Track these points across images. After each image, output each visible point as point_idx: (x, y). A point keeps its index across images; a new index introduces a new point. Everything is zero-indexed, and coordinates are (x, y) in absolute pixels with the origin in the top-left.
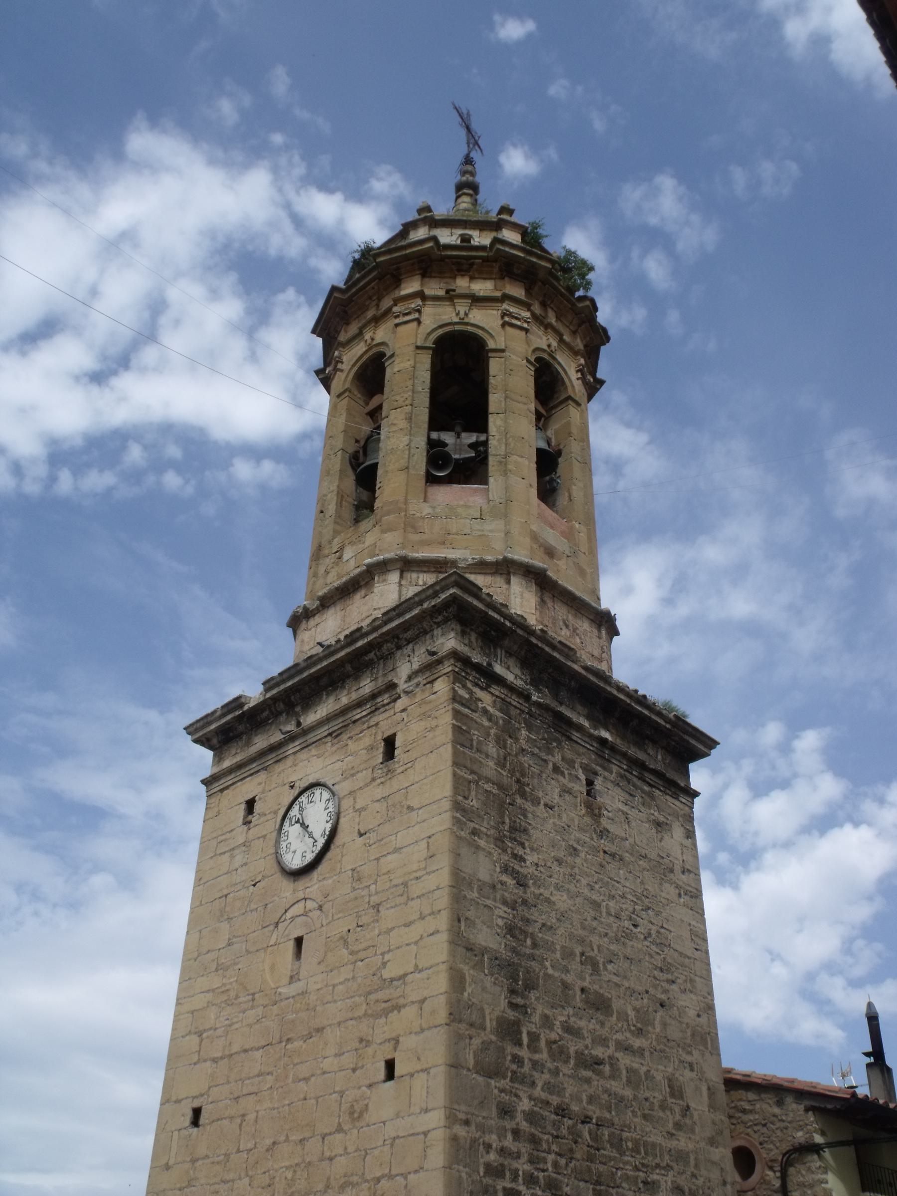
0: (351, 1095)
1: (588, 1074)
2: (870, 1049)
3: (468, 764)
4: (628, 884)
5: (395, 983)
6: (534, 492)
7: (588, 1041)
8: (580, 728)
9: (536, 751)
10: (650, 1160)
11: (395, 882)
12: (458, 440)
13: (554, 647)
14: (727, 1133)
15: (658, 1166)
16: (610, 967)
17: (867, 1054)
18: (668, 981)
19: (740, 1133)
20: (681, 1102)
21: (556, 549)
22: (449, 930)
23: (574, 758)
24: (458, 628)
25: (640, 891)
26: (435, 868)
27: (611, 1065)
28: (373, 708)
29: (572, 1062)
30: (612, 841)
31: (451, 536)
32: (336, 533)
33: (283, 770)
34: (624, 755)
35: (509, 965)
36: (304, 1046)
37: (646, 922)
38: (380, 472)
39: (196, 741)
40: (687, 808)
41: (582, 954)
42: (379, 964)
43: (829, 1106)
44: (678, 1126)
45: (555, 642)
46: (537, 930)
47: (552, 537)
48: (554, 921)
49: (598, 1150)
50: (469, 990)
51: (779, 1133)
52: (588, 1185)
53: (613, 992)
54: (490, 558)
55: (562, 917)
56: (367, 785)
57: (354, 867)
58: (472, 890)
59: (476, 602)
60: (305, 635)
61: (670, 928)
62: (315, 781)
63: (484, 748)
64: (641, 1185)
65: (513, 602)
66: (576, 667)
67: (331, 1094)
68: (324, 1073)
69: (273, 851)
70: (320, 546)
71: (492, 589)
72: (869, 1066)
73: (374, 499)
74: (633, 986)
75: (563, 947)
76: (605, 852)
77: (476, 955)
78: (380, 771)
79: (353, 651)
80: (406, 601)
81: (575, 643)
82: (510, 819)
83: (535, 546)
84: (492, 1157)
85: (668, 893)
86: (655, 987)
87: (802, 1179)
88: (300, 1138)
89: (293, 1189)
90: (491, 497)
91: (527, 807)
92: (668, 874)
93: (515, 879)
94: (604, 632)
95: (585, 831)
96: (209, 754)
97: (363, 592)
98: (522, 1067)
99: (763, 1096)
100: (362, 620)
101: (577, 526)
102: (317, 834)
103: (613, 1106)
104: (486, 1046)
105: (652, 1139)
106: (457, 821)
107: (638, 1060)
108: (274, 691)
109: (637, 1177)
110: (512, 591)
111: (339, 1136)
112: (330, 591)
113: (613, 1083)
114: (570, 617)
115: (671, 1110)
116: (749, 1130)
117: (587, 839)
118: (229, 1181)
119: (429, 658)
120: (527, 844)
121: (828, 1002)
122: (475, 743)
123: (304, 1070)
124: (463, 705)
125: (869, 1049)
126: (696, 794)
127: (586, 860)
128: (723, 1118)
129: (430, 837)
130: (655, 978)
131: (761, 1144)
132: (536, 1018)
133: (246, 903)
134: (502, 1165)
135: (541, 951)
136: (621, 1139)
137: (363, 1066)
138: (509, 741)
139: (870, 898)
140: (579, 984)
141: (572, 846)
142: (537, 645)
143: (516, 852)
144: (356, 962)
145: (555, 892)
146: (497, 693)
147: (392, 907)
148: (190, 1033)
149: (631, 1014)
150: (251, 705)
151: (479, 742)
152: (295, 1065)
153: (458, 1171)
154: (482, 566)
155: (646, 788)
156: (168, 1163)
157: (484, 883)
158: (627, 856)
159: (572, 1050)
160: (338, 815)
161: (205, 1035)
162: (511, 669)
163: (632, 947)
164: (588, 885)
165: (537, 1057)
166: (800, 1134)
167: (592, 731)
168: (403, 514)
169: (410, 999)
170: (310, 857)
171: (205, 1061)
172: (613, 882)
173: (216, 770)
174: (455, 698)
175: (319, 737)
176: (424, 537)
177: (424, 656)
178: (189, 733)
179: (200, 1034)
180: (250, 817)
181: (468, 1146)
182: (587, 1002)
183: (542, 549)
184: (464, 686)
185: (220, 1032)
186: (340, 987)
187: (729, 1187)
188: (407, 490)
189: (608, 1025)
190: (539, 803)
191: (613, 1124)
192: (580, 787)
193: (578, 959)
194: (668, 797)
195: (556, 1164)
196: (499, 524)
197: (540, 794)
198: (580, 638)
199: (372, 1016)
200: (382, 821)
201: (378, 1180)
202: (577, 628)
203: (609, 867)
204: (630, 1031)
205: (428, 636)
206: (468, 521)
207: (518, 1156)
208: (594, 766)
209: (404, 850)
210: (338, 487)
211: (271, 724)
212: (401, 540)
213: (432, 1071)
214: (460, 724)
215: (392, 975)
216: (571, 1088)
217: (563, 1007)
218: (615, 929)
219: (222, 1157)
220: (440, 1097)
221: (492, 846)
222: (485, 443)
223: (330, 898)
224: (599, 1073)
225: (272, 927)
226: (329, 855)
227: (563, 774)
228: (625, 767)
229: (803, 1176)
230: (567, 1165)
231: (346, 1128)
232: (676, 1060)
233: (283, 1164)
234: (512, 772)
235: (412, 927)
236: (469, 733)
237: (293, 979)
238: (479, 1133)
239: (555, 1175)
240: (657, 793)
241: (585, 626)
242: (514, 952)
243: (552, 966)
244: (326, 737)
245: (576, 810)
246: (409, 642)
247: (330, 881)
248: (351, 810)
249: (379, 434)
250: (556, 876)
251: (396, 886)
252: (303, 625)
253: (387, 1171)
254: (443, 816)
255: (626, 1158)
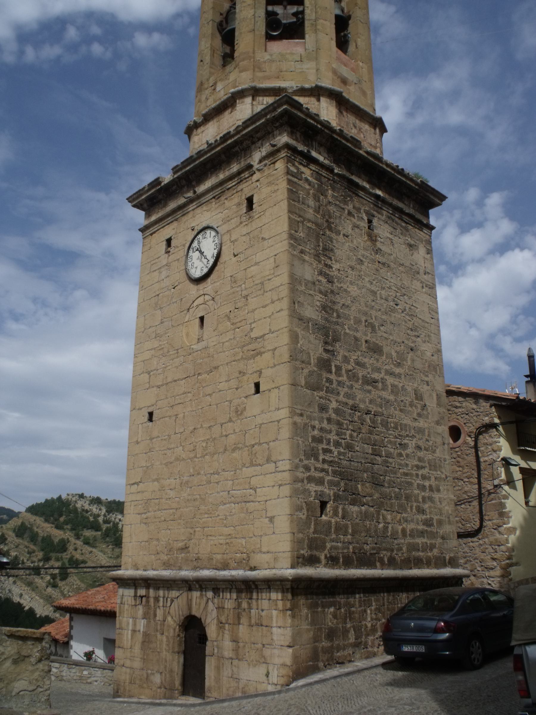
0: (236, 402)
1: (370, 388)
2: (528, 373)
3: (297, 211)
4: (392, 281)
5: (258, 340)
6: (334, 43)
7: (370, 370)
8: (363, 189)
9: (338, 203)
10: (403, 433)
11: (256, 282)
12: (285, 11)
13: (347, 140)
14: (446, 418)
15: (407, 436)
16: (382, 328)
17: (527, 376)
18: (415, 336)
19: (454, 419)
20: (421, 402)
21: (348, 79)
22: (289, 309)
23: (361, 207)
24: (289, 129)
25: (400, 285)
26: (279, 274)
27: (383, 383)
28: (239, 180)
29: (360, 381)
30: (383, 256)
31: (283, 73)
32: (211, 74)
33: (187, 220)
34: (391, 205)
35: (324, 328)
36: (208, 377)
37: (403, 303)
38: (237, 34)
39: (134, 206)
40: (427, 236)
41: (366, 321)
42: (249, 329)
43: (504, 404)
44: (419, 415)
45: (348, 137)
46: (339, 308)
47: (345, 72)
48: (349, 302)
49: (375, 428)
50: (301, 342)
51: (475, 418)
52: (369, 446)
53: (384, 343)
54: (307, 86)
55: (354, 300)
56: (237, 226)
57: (231, 274)
58: (301, 285)
59: (299, 114)
60: (195, 139)
61: (417, 306)
62: (206, 225)
63: (307, 202)
64: (398, 446)
65: (322, 113)
66: (361, 152)
67: (225, 402)
68: (220, 391)
69: (184, 268)
70: (202, 83)
71: (309, 105)
72: (527, 382)
73: (233, 51)
74: (395, 339)
75: (355, 317)
76: (379, 262)
77: (304, 323)
78: (245, 218)
79: (226, 146)
80: (257, 114)
81: (360, 137)
82: (323, 244)
83: (335, 78)
84: (316, 432)
85: (416, 286)
86: (408, 339)
87: (486, 441)
88: (208, 426)
89: (207, 452)
90: (307, 47)
91: (332, 236)
92: (416, 275)
93: (326, 278)
94: (378, 130)
95: (368, 250)
96: (143, 213)
97: (230, 110)
98: (332, 384)
99: (467, 399)
100: (230, 127)
101: (361, 64)
102: (209, 256)
103: (383, 405)
104: (311, 373)
105: (405, 422)
106: (291, 245)
107: (398, 380)
108: (179, 174)
109: (396, 442)
110: (321, 106)
111: (230, 424)
112: (210, 111)
113: (383, 392)
114: (357, 121)
115: (416, 406)
116: (458, 417)
117: (369, 255)
118: (171, 449)
119: (272, 148)
120: (333, 258)
121: (502, 350)
122: (301, 199)
123: (209, 390)
124: (293, 176)
125: (528, 373)
126: (432, 228)
127: (368, 267)
128: (444, 410)
129: (276, 255)
130: (408, 335)
131: (465, 424)
132: (340, 358)
133: (170, 299)
134: (321, 437)
135: (342, 320)
136: (388, 422)
137: (242, 387)
138: (322, 197)
139: (528, 292)
140: (364, 338)
141: (360, 259)
142: (337, 139)
143: (326, 263)
144: (235, 329)
145: (350, 286)
146: (314, 169)
147: (255, 297)
148: (143, 373)
149: (394, 354)
150: (166, 182)
151: (303, 198)
152: (203, 387)
153: (297, 440)
154: (303, 91)
155: (404, 224)
156: (137, 441)
157: (308, 281)
158: (392, 265)
159: (360, 375)
160: (221, 245)
161: (152, 373)
162: (322, 153)
163: (395, 317)
164: (369, 281)
165: (340, 379)
166: (487, 418)
167: (371, 190)
168: (252, 60)
169: (267, 349)
170: (205, 270)
171: (153, 387)
172: (384, 280)
173: (146, 222)
174: (288, 172)
175: (207, 199)
176: (266, 74)
177: (268, 147)
178: (130, 202)
179: (149, 373)
180: (169, 249)
181: (302, 426)
182: (369, 348)
183: (339, 79)
184: (294, 165)
185: (160, 371)
186: (227, 344)
187: (446, 446)
188: (254, 44)
189: (381, 361)
190: (340, 234)
191: (383, 414)
192: (364, 224)
193: (363, 324)
194: (416, 230)
195: (351, 436)
196: (312, 65)
197: (340, 228)
198: (363, 134)
199: (245, 359)
200: (247, 247)
201: (253, 446)
202: (361, 128)
203: (381, 271)
204: (394, 364)
205: (271, 136)
206: (293, 63)
207: (330, 432)
208: (372, 211)
209: (261, 263)
210: (211, 44)
211: (178, 193)
212: (251, 77)
213: (281, 388)
214: (291, 188)
215: (257, 336)
216: (359, 396)
217: (355, 351)
218: (385, 307)
219: (167, 437)
220: (286, 401)
221: (313, 260)
222: (302, 12)
223: (218, 293)
224: (376, 387)
225: (185, 312)
226: (217, 268)
227: (354, 216)
228: (391, 212)
229: (487, 439)
230: (357, 436)
231: (234, 419)
232: (419, 380)
233: (200, 439)
234: (323, 216)
235: (267, 308)
236: (297, 193)
237: (199, 340)
238: (308, 420)
239: (350, 441)
240: (410, 227)
241: (366, 127)
242: (326, 320)
243: (349, 328)
244: (211, 199)
245: (362, 237)
246: (259, 139)
247: (218, 284)
248: (228, 242)
249: (235, 8)
250: (350, 276)
251: (257, 284)
252: (195, 132)
253: (257, 441)
254: (284, 242)
255: (390, 432)
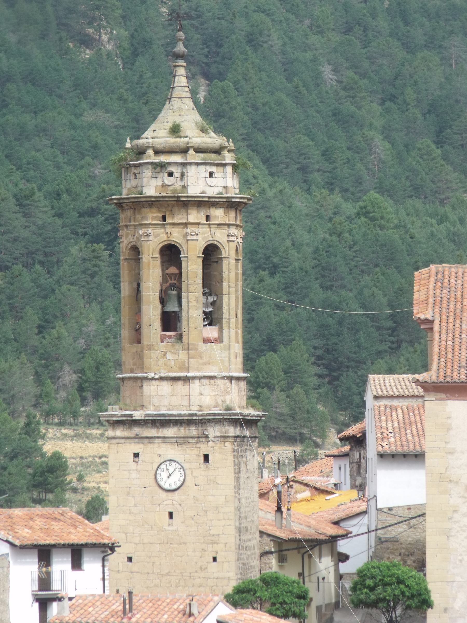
226: (182, 488)
